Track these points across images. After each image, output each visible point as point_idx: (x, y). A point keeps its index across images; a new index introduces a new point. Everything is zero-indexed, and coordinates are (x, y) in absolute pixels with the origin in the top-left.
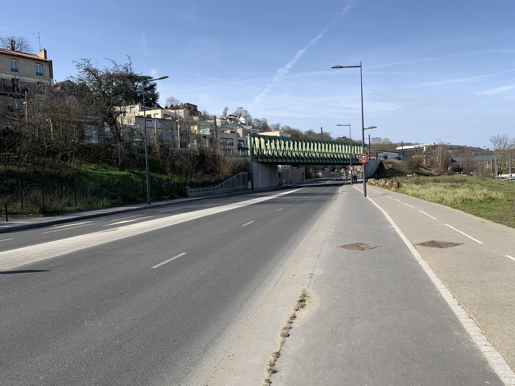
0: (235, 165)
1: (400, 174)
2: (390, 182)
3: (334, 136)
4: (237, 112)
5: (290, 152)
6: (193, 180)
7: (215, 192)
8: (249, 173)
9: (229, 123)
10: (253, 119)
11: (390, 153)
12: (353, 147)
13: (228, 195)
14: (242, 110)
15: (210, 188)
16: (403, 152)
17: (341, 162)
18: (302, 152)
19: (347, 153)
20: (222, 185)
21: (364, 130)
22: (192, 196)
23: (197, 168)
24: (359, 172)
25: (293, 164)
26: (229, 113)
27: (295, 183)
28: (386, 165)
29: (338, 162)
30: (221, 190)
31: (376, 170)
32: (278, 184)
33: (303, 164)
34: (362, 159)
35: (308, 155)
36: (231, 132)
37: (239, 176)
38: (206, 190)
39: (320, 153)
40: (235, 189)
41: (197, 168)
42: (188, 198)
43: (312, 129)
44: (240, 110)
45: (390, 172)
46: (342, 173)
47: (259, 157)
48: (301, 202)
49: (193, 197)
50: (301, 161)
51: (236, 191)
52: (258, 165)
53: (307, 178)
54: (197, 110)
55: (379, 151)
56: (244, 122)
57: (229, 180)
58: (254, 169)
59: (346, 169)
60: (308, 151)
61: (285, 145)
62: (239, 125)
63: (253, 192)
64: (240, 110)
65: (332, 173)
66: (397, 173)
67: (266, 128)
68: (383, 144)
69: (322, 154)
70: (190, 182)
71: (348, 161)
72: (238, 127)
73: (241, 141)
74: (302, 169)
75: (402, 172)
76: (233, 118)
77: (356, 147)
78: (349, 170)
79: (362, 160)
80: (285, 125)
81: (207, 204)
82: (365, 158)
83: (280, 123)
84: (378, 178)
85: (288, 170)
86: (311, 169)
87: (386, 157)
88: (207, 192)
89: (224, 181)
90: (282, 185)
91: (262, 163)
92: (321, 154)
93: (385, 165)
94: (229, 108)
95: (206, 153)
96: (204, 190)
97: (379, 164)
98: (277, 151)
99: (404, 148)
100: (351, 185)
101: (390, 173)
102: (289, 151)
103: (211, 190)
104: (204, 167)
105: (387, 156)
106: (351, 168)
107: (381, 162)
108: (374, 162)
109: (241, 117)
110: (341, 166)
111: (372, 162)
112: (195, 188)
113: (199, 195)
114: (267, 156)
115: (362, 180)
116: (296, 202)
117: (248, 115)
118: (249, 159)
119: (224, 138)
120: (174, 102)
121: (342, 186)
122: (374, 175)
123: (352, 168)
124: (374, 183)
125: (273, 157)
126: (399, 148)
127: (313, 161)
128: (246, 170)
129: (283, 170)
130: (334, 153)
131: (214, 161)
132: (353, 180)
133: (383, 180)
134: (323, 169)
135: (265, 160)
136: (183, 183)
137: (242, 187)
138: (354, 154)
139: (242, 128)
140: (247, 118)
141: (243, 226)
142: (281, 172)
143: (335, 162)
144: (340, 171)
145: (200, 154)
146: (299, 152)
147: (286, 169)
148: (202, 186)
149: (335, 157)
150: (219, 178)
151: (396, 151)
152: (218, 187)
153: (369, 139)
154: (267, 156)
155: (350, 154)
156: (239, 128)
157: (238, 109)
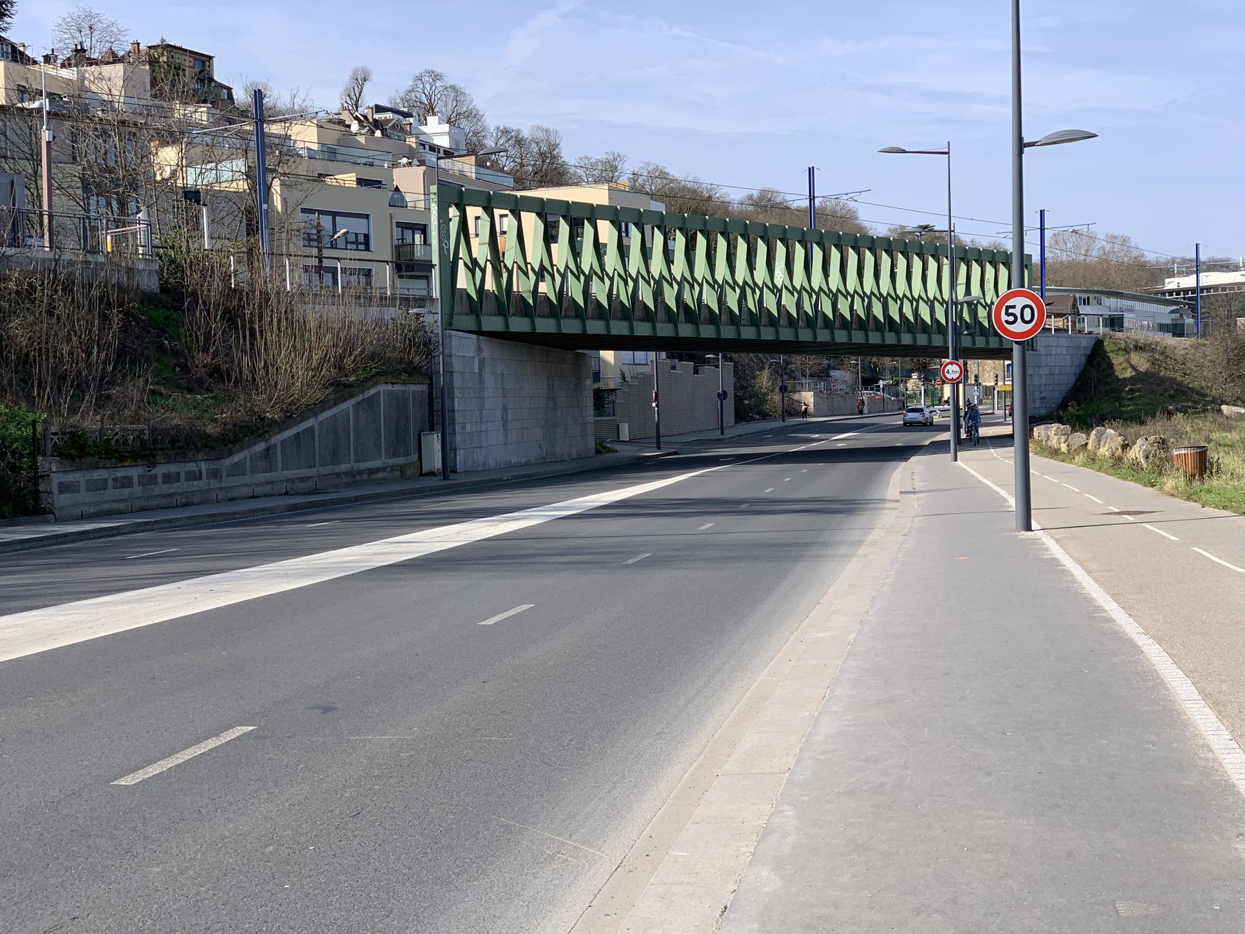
0: (350, 344)
1: (1187, 401)
2: (1152, 445)
3: (878, 223)
4: (413, 94)
5: (649, 284)
6: (90, 423)
7: (220, 489)
8: (431, 386)
9: (362, 139)
10: (492, 129)
11: (1138, 305)
12: (963, 268)
13: (295, 507)
14: (438, 83)
15: (192, 467)
16: (1192, 300)
17: (906, 339)
18: (713, 288)
19: (935, 298)
20: (268, 449)
21: (1021, 153)
22: (77, 512)
23: (126, 358)
24: (989, 391)
25: (678, 348)
26: (371, 98)
27: (679, 439)
28: (1122, 359)
29: (891, 339)
30: (261, 477)
31: (1072, 380)
32: (591, 444)
33: (717, 345)
34: (1007, 314)
35: (742, 299)
36: (360, 182)
37: (372, 402)
38: (168, 478)
39: (799, 293)
40: (348, 473)
41: (126, 358)
42: (47, 522)
43: (774, 187)
44: (428, 86)
45: (1139, 390)
46: (910, 397)
47: (488, 306)
48: (663, 559)
49: (82, 518)
50: (707, 332)
51: (348, 485)
52: (479, 350)
53: (742, 415)
54: (211, 80)
55: (1086, 296)
56: (444, 142)
57: (311, 422)
58: (457, 366)
59: (928, 376)
60: (741, 284)
61: (646, 253)
62: (410, 154)
63: (449, 486)
64: (428, 86)
65: (866, 395)
66: (1172, 397)
67: (555, 174)
68: (1104, 261)
69: (810, 296)
70: (64, 433)
71: (940, 337)
72: (405, 160)
73: (413, 227)
74: (720, 375)
75: (1198, 393)
76: (390, 121)
77: (976, 268)
78: (944, 382)
79: (1011, 319)
80: (648, 164)
81: (123, 561)
82: (1027, 311)
83: (622, 154)
84: (1083, 423)
85: (647, 378)
86: (766, 373)
87: (1115, 322)
88: (176, 487)
89: (281, 430)
90: (609, 450)
91: (504, 336)
92: (805, 296)
93: (1117, 360)
94: (374, 77)
95: (192, 279)
96: (153, 480)
97: (1089, 352)
98: (582, 278)
99: (1210, 279)
100: (950, 456)
101: (1140, 397)
102: (643, 277)
103: (200, 478)
104: (175, 353)
105: (1121, 319)
106: (953, 371)
107: (1099, 344)
108: (1064, 342)
109: (430, 119)
110: (908, 362)
111: (1053, 342)
112: (97, 468)
113: (122, 506)
114: (531, 301)
115: (1007, 430)
116: (630, 562)
117: (465, 109)
118: (433, 319)
119: (320, 212)
120: (96, 35)
121: (906, 459)
122: (1064, 405)
123: (955, 368)
124: (1064, 448)
125: (560, 307)
126: (1176, 280)
127: (767, 334)
128: (412, 372)
129: (624, 378)
130: (872, 293)
131: (231, 317)
132: (962, 431)
133: (1110, 431)
134: (822, 375)
135: (519, 325)
136: (26, 439)
137: (391, 461)
138: (968, 299)
139: (424, 168)
140: (464, 123)
141: (122, 782)
142: (612, 387)
143: (875, 338)
144: (902, 386)
145: (164, 288)
146: (697, 288)
147: (640, 369)
148: (143, 457)
149: (875, 313)
150: (251, 412)
151: (1163, 293)
152: (243, 461)
153: (1042, 229)
154: (531, 301)
155: (947, 303)
156: (410, 164)
157: (419, 78)
